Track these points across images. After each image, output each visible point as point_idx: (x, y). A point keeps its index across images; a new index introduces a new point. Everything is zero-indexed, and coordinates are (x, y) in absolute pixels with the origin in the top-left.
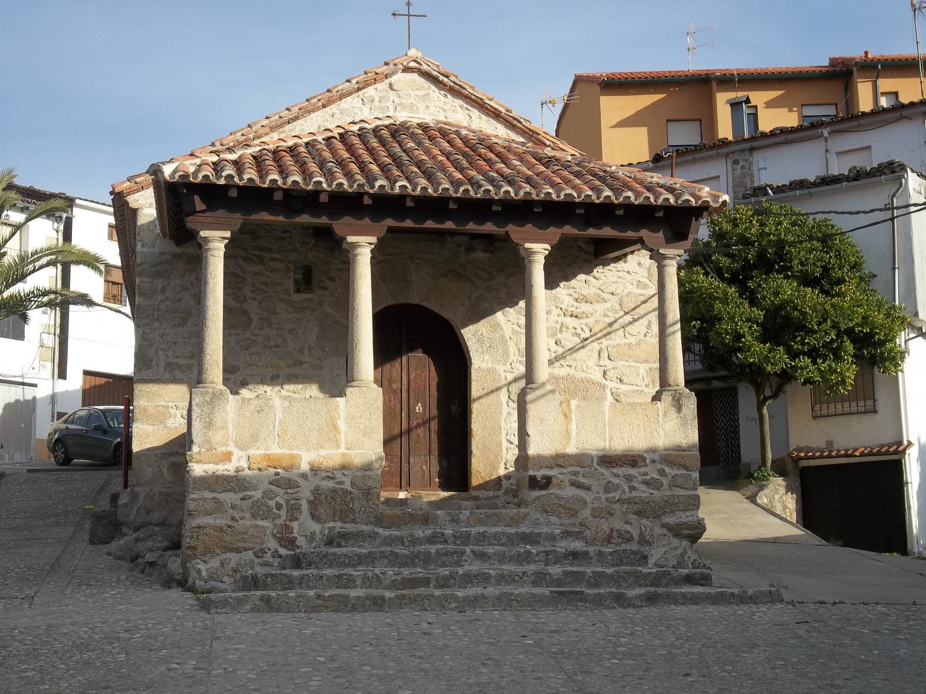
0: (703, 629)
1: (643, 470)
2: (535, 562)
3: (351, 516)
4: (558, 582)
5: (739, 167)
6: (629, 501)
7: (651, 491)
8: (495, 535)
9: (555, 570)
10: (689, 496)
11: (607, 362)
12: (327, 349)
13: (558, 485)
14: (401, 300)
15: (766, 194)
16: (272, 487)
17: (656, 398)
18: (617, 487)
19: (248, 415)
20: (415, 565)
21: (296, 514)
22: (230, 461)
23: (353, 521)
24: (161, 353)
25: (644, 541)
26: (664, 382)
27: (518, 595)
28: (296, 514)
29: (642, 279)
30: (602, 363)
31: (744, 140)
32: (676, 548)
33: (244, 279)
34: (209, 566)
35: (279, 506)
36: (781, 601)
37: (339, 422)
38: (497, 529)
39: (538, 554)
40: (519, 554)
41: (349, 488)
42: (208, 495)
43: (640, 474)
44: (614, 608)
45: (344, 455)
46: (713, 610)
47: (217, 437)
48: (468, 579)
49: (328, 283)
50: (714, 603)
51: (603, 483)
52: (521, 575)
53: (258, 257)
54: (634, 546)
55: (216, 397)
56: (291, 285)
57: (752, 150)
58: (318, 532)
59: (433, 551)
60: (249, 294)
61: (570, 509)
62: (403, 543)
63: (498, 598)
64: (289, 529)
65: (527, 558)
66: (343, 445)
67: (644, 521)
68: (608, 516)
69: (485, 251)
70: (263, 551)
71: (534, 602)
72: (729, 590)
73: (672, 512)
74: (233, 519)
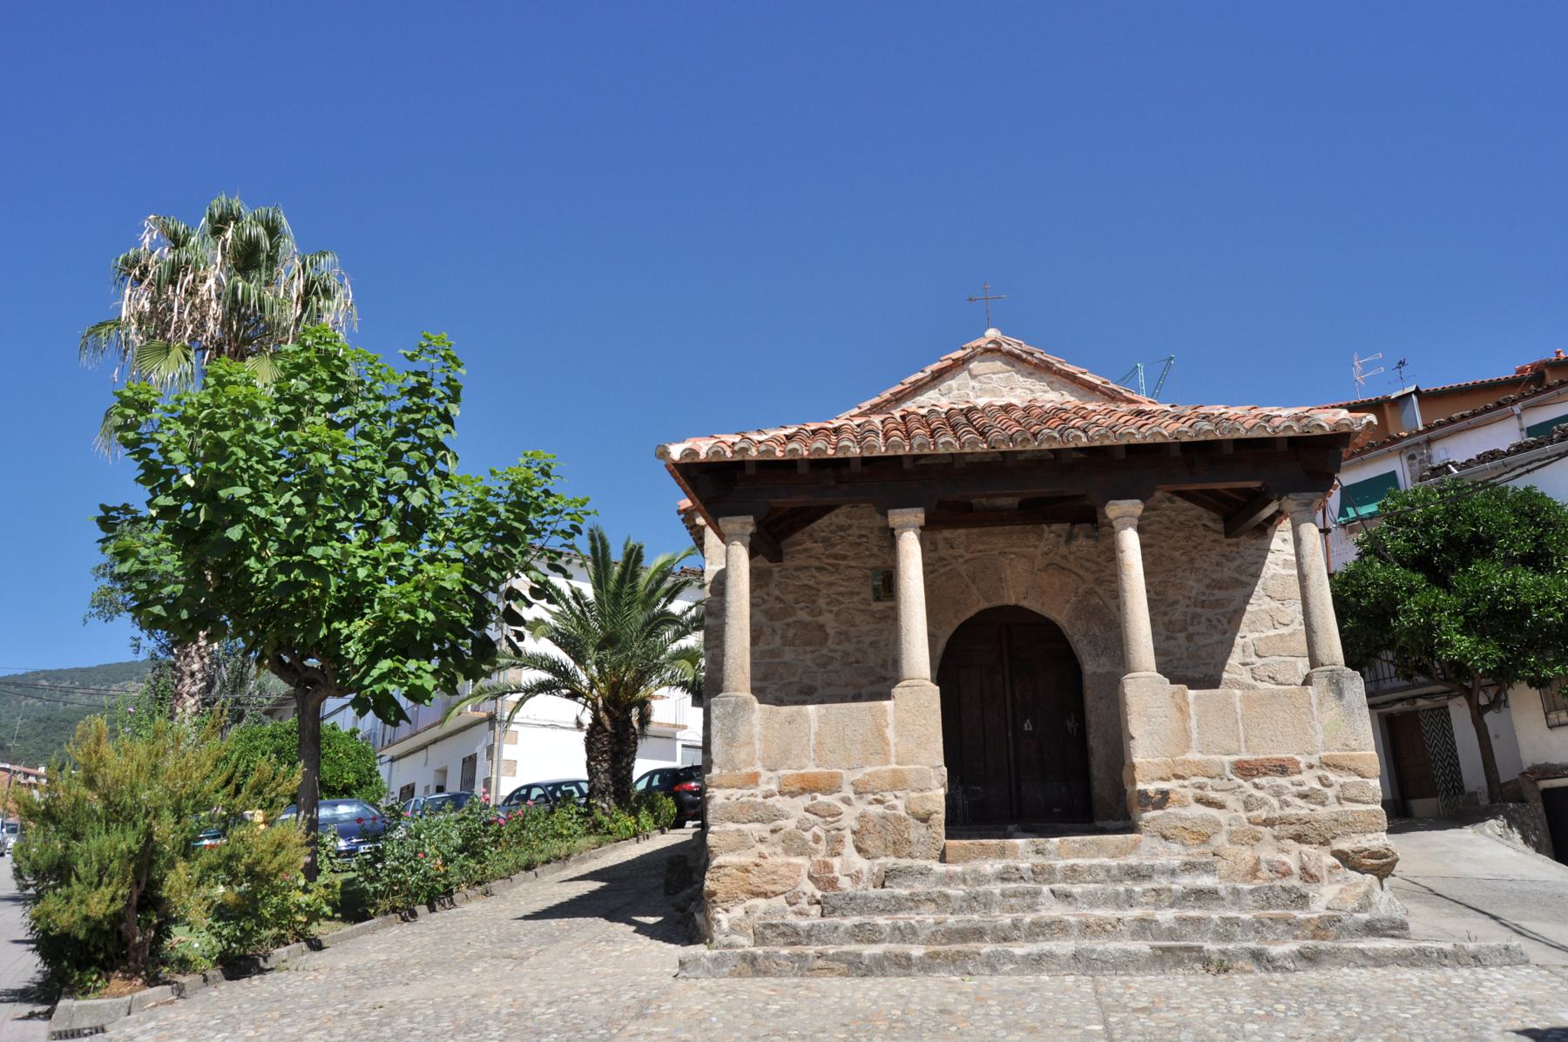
0: (1391, 1009)
1: (1296, 778)
2: (1141, 904)
3: (908, 850)
4: (1171, 933)
5: (1416, 462)
6: (1283, 821)
8: (1090, 869)
9: (1166, 916)
10: (1369, 812)
11: (1254, 659)
13: (1179, 801)
14: (996, 603)
15: (1449, 471)
16: (808, 815)
17: (1307, 681)
18: (1263, 803)
19: (777, 726)
20: (973, 911)
21: (838, 847)
22: (757, 785)
23: (910, 855)
25: (1308, 875)
27: (1101, 953)
28: (838, 847)
30: (1248, 660)
31: (1419, 433)
32: (1357, 885)
34: (731, 915)
35: (817, 839)
36: (1527, 962)
38: (1095, 861)
39: (1144, 894)
40: (1117, 894)
41: (903, 814)
42: (731, 826)
44: (1251, 972)
45: (894, 771)
46: (1411, 976)
47: (741, 755)
48: (1040, 930)
50: (1413, 965)
51: (1243, 797)
52: (1114, 922)
53: (833, 566)
54: (1294, 882)
55: (741, 706)
56: (867, 593)
57: (1429, 442)
58: (865, 870)
59: (997, 891)
60: (824, 606)
61: (1199, 833)
62: (964, 881)
63: (1075, 956)
64: (828, 867)
65: (1130, 900)
66: (893, 759)
67: (1305, 848)
69: (1088, 537)
70: (797, 896)
71: (1127, 963)
72: (1436, 945)
73: (1346, 834)
74: (762, 856)
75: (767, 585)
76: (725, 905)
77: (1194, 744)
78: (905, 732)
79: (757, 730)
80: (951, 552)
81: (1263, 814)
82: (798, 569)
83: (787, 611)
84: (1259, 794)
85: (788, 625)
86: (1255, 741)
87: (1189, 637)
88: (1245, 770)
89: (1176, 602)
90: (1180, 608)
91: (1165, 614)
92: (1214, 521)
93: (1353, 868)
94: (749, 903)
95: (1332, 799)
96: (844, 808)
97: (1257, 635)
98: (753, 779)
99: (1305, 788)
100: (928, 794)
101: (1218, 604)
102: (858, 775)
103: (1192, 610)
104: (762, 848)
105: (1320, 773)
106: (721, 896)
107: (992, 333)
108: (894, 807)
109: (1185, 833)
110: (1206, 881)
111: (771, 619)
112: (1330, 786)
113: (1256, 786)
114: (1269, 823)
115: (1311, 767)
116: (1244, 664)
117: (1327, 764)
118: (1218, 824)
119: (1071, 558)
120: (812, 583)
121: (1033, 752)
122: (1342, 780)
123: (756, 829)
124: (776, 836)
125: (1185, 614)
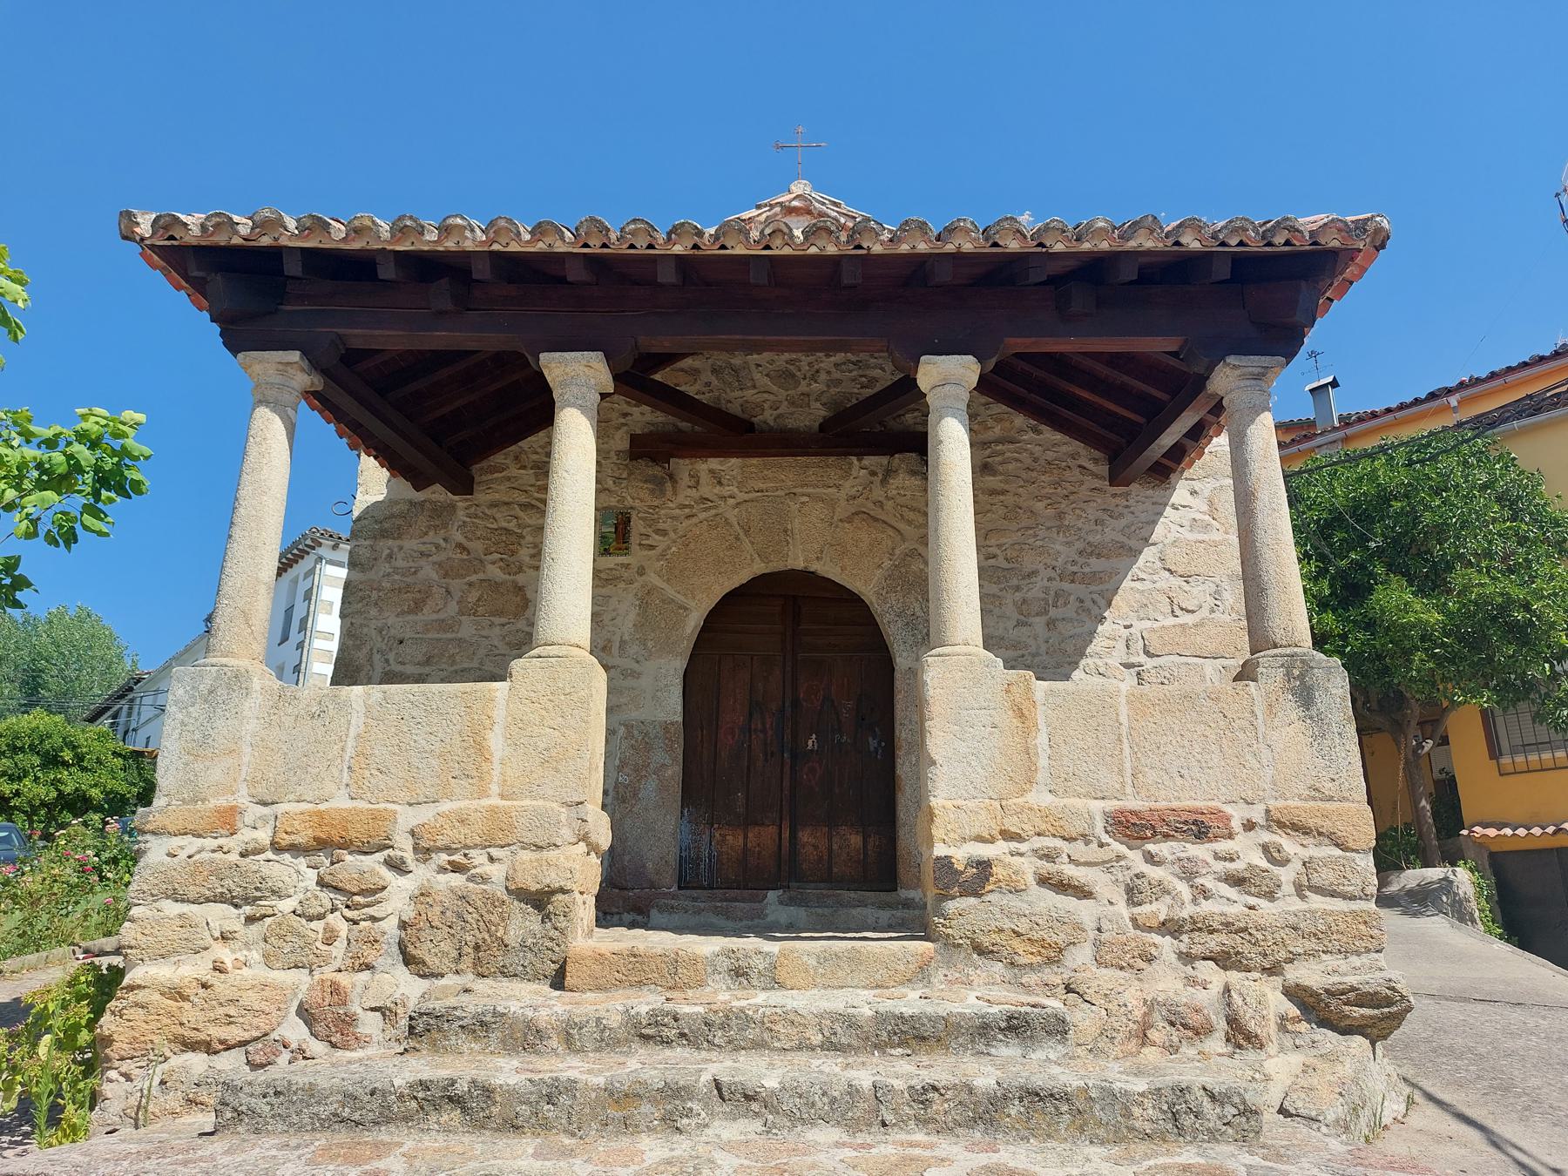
1: (1223, 846)
6: (1198, 926)
7: (1252, 901)
11: (1142, 658)
12: (650, 644)
14: (776, 565)
17: (1246, 673)
19: (288, 721)
24: (377, 657)
26: (1260, 640)
29: (1198, 516)
30: (1133, 660)
31: (1335, 429)
33: (522, 537)
37: (490, 735)
42: (171, 908)
43: (1217, 857)
45: (493, 810)
49: (656, 539)
66: (495, 789)
67: (1234, 976)
68: (1140, 964)
69: (913, 473)
74: (219, 968)
75: (445, 526)
76: (126, 1066)
77: (1041, 776)
78: (544, 742)
79: (252, 726)
80: (717, 490)
81: (1158, 910)
82: (494, 505)
83: (476, 564)
84: (1155, 873)
85: (470, 584)
86: (1152, 776)
87: (1051, 624)
88: (1132, 828)
89: (1034, 573)
90: (1040, 582)
91: (1018, 588)
92: (1096, 461)
93: (1324, 1023)
94: (175, 1061)
95: (1288, 888)
96: (388, 875)
97: (1148, 624)
98: (228, 821)
99: (1238, 866)
100: (551, 854)
101: (1095, 578)
102: (425, 815)
103: (1056, 585)
104: (225, 954)
105: (1266, 837)
106: (120, 1046)
107: (800, 187)
108: (485, 880)
109: (1016, 943)
110: (1045, 1065)
111: (446, 575)
112: (1284, 862)
113: (1150, 859)
114: (1171, 928)
115: (1249, 826)
116: (1128, 666)
117: (1277, 823)
118: (1079, 927)
119: (889, 505)
120: (512, 525)
121: (782, 780)
122: (1305, 853)
123: (222, 916)
124: (255, 928)
125: (1046, 591)
